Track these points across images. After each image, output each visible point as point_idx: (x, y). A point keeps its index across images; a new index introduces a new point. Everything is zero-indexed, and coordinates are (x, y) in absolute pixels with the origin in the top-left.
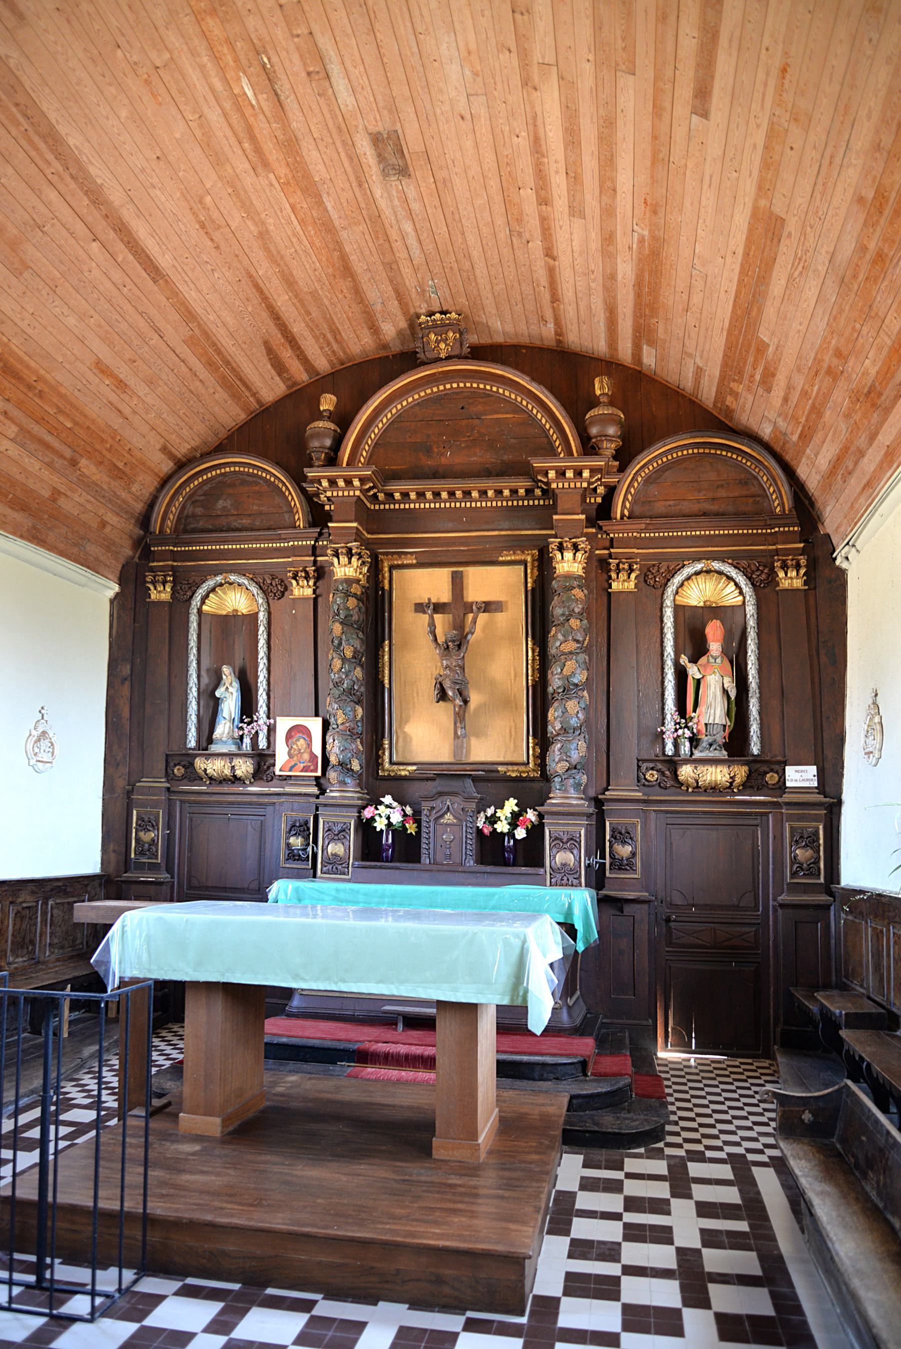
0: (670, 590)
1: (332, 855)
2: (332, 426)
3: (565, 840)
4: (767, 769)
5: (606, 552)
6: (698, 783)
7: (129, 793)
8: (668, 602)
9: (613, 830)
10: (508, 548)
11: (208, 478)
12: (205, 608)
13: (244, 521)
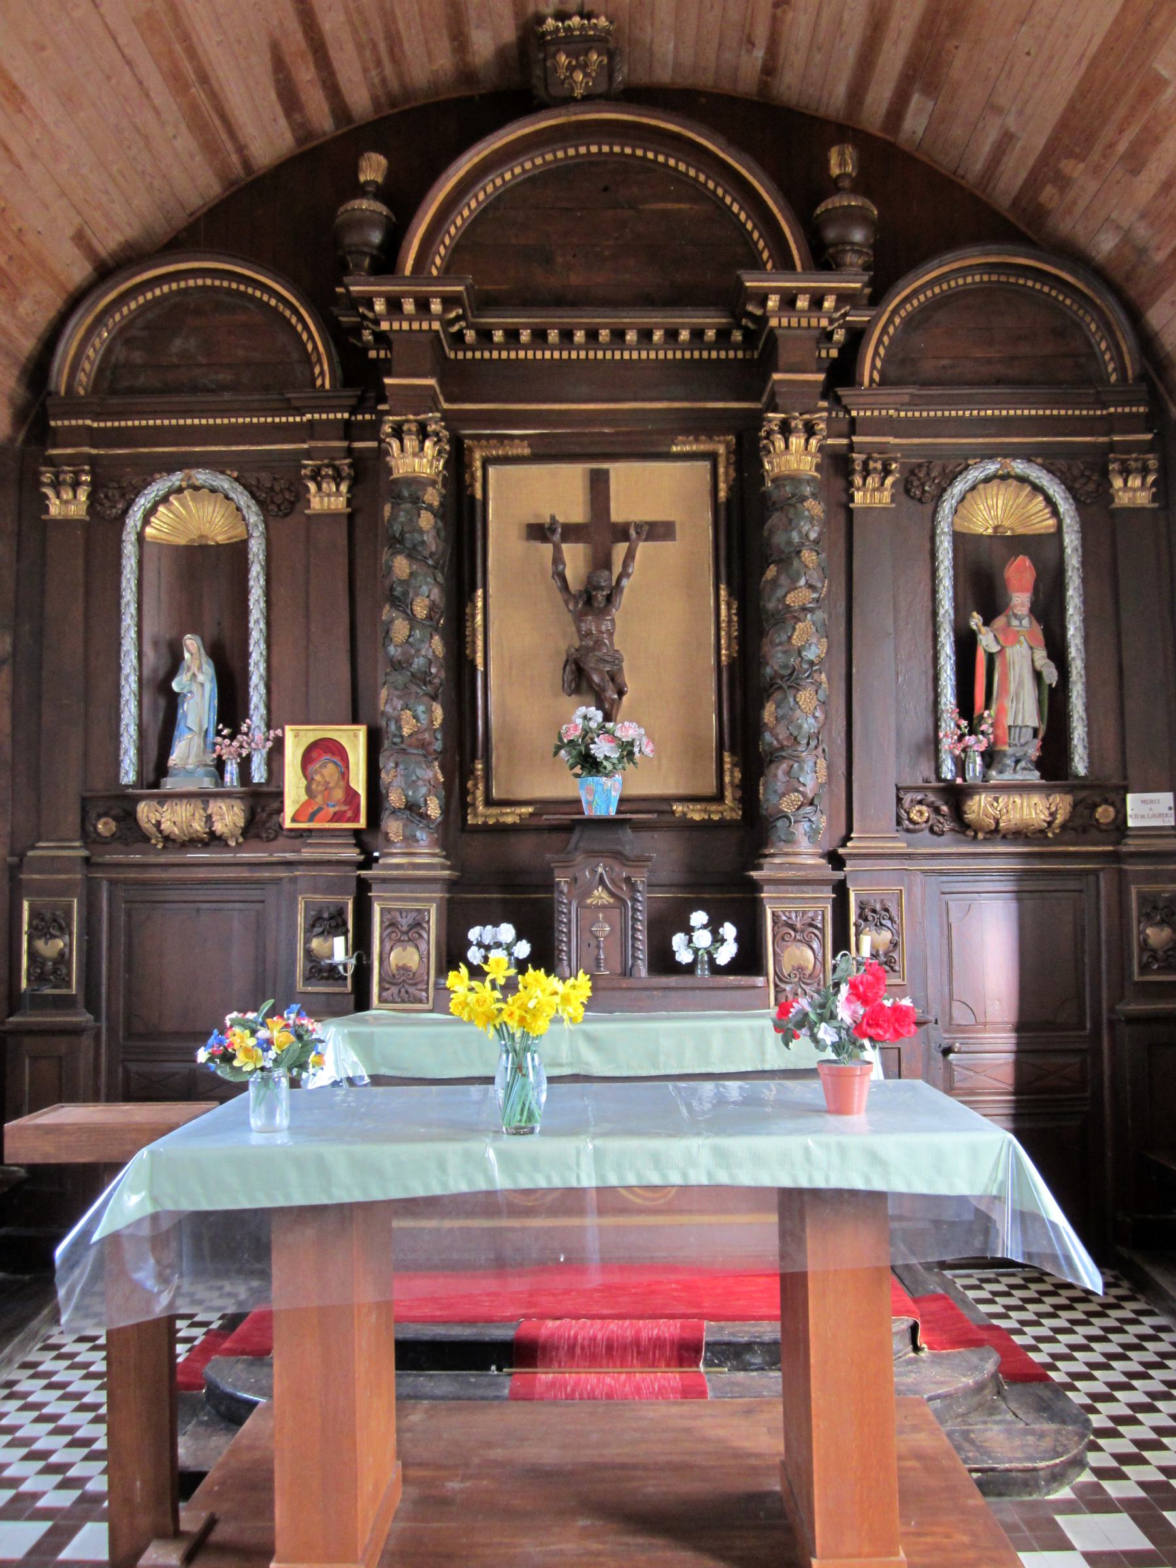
0: (947, 507)
1: (398, 968)
2: (383, 209)
3: (799, 926)
4: (1097, 800)
5: (845, 441)
6: (997, 823)
7: (14, 871)
8: (944, 527)
9: (862, 907)
10: (686, 432)
11: (155, 298)
12: (149, 531)
13: (221, 376)
